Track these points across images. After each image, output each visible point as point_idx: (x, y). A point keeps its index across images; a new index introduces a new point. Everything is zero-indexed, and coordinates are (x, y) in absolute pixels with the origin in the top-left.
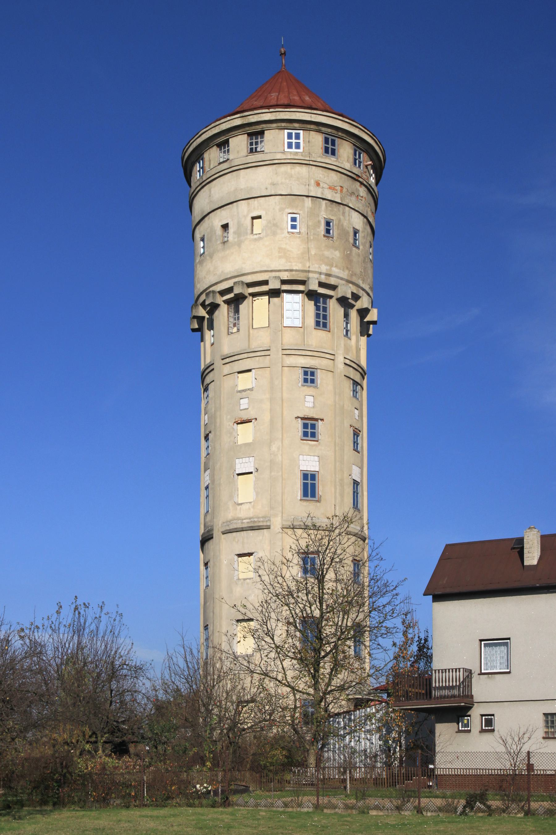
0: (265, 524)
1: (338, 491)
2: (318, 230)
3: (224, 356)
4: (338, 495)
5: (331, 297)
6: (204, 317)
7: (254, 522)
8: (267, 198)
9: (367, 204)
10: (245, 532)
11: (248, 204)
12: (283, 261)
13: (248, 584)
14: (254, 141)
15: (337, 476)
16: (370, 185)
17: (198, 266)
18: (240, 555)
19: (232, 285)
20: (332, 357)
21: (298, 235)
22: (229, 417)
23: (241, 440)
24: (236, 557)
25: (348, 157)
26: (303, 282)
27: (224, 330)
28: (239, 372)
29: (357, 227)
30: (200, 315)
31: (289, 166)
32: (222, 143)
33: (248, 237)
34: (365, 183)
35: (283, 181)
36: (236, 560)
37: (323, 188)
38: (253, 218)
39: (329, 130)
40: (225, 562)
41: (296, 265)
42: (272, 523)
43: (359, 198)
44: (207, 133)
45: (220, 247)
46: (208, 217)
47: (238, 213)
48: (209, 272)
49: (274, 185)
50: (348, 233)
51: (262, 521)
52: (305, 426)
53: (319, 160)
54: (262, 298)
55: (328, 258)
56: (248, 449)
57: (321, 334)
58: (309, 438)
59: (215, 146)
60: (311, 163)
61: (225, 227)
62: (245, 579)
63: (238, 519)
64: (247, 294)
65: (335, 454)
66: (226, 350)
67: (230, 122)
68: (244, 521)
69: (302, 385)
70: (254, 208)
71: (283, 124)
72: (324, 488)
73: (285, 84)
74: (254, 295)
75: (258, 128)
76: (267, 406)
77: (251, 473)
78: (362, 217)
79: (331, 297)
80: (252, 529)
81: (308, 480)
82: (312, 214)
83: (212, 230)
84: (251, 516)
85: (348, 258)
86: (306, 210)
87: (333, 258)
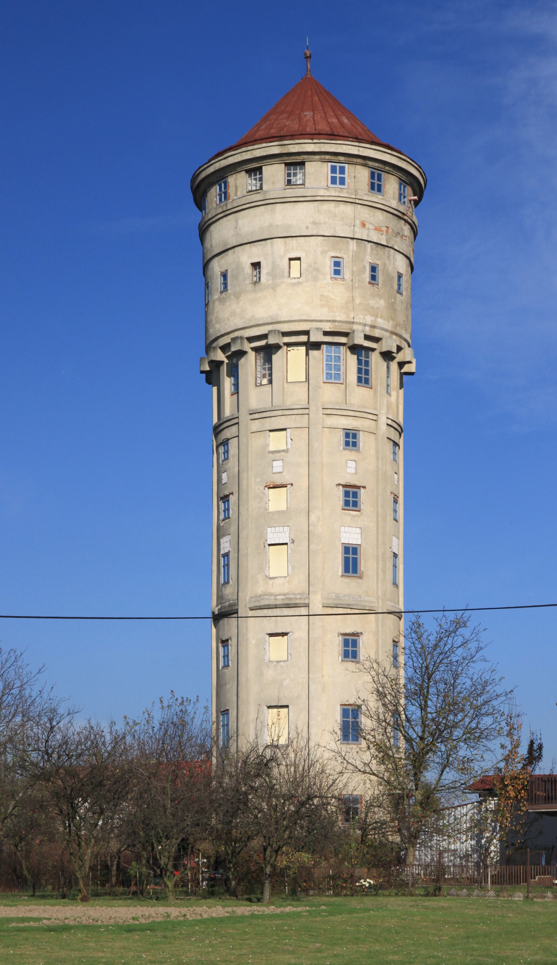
0: (303, 601)
1: (380, 566)
2: (363, 276)
3: (252, 410)
4: (380, 571)
5: (373, 350)
6: (222, 362)
7: (290, 599)
10: (278, 609)
11: (286, 243)
12: (325, 310)
13: (282, 667)
14: (292, 172)
15: (380, 550)
16: (413, 222)
17: (217, 303)
18: (271, 635)
20: (374, 417)
21: (342, 282)
22: (258, 480)
23: (272, 507)
24: (267, 636)
25: (394, 194)
26: (346, 335)
27: (251, 381)
28: (270, 431)
30: (219, 359)
31: (333, 204)
32: (254, 168)
33: (285, 280)
34: (409, 221)
36: (267, 640)
37: (369, 229)
38: (291, 259)
39: (376, 165)
40: (254, 642)
41: (339, 316)
42: (311, 601)
43: (404, 238)
44: (235, 156)
45: (250, 287)
46: (232, 250)
47: (273, 252)
48: (233, 314)
49: (315, 224)
50: (393, 278)
51: (300, 599)
52: (347, 494)
53: (365, 198)
54: (299, 348)
55: (373, 307)
56: (281, 518)
57: (363, 391)
58: (351, 508)
59: (244, 172)
60: (357, 201)
61: (256, 265)
62: (278, 662)
63: (271, 594)
64: (282, 344)
65: (378, 526)
67: (265, 149)
68: (278, 597)
69: (344, 449)
71: (327, 157)
72: (367, 563)
73: (317, 98)
74: (288, 345)
75: (299, 159)
77: (286, 544)
78: (405, 259)
79: (373, 350)
80: (288, 606)
81: (349, 554)
82: (356, 258)
83: (239, 267)
84: (286, 591)
85: (392, 307)
86: (351, 254)
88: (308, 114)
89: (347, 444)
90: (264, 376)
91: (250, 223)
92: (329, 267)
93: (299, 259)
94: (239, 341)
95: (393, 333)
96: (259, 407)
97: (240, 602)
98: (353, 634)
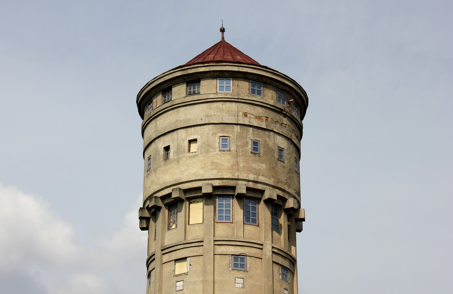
8: (202, 127)
9: (291, 130)
11: (187, 131)
12: (215, 172)
16: (292, 116)
19: (171, 191)
29: (282, 146)
31: (221, 103)
35: (216, 113)
37: (250, 118)
38: (190, 142)
41: (227, 175)
45: (163, 163)
48: (153, 182)
49: (207, 116)
53: (246, 98)
55: (255, 169)
57: (250, 228)
60: (240, 100)
61: (167, 149)
66: (167, 243)
70: (191, 134)
82: (240, 136)
83: (157, 151)
86: (236, 134)
87: (260, 169)
89: (236, 265)
92: (217, 141)
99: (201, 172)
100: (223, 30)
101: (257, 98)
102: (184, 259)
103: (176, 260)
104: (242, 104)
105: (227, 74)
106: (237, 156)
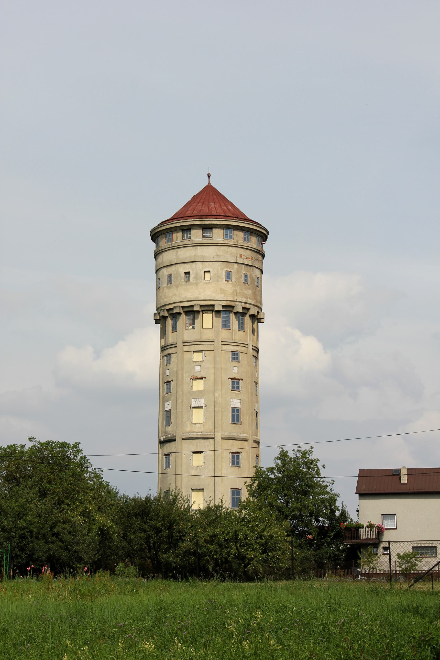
0: (211, 436)
8: (214, 263)
12: (222, 295)
13: (200, 469)
18: (194, 453)
20: (246, 346)
22: (187, 375)
31: (226, 247)
35: (223, 254)
38: (205, 272)
48: (175, 295)
52: (233, 383)
56: (199, 394)
57: (241, 333)
62: (198, 466)
63: (194, 432)
68: (198, 434)
70: (206, 267)
76: (212, 371)
82: (237, 271)
83: (178, 273)
86: (235, 270)
88: (212, 204)
89: (233, 358)
90: (190, 325)
91: (185, 254)
92: (223, 275)
93: (209, 271)
94: (178, 308)
95: (255, 306)
96: (188, 340)
97: (177, 435)
98: (237, 453)
99: (214, 295)
100: (209, 176)
101: (248, 244)
102: (201, 351)
103: (194, 351)
104: (239, 248)
105: (230, 227)
106: (236, 285)
